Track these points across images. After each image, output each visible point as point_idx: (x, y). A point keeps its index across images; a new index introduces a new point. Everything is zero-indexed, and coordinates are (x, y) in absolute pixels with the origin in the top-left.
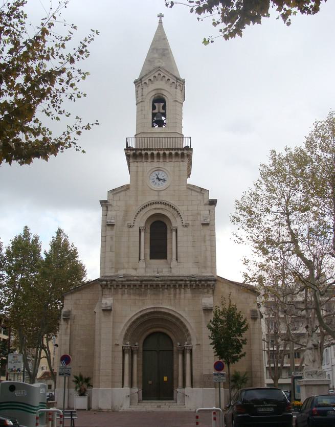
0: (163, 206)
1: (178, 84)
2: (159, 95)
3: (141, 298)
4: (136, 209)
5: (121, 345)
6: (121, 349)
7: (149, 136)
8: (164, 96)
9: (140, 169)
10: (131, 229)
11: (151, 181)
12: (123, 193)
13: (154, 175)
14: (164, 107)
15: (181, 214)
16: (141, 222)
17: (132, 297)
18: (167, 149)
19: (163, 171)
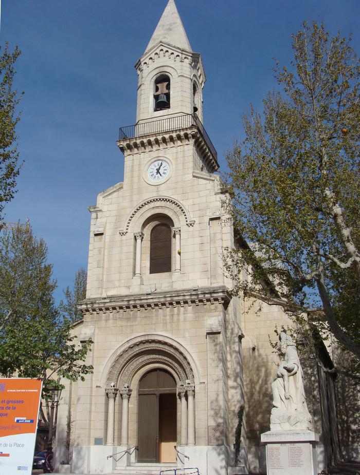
0: (163, 203)
1: (184, 56)
2: (162, 73)
3: (129, 324)
4: (130, 211)
5: (104, 387)
6: (104, 393)
7: (151, 120)
8: (167, 74)
9: (136, 162)
10: (124, 237)
11: (149, 175)
12: (115, 194)
13: (153, 167)
14: (168, 87)
15: (185, 210)
16: (136, 226)
17: (119, 323)
18: (166, 132)
19: (168, 164)
